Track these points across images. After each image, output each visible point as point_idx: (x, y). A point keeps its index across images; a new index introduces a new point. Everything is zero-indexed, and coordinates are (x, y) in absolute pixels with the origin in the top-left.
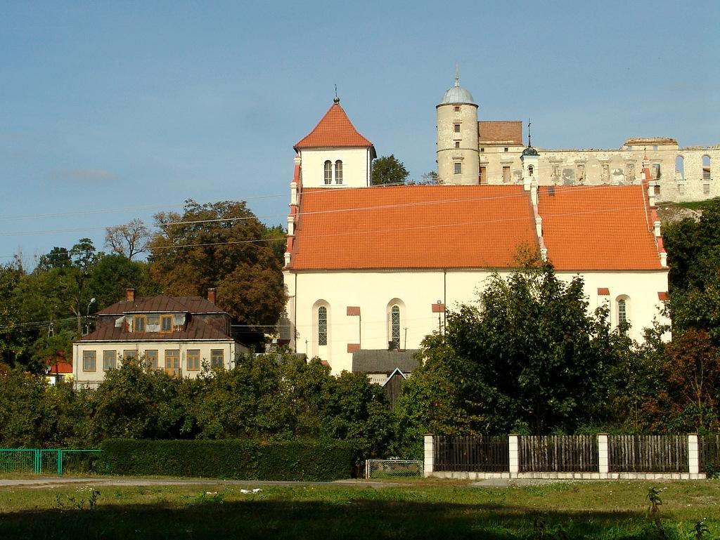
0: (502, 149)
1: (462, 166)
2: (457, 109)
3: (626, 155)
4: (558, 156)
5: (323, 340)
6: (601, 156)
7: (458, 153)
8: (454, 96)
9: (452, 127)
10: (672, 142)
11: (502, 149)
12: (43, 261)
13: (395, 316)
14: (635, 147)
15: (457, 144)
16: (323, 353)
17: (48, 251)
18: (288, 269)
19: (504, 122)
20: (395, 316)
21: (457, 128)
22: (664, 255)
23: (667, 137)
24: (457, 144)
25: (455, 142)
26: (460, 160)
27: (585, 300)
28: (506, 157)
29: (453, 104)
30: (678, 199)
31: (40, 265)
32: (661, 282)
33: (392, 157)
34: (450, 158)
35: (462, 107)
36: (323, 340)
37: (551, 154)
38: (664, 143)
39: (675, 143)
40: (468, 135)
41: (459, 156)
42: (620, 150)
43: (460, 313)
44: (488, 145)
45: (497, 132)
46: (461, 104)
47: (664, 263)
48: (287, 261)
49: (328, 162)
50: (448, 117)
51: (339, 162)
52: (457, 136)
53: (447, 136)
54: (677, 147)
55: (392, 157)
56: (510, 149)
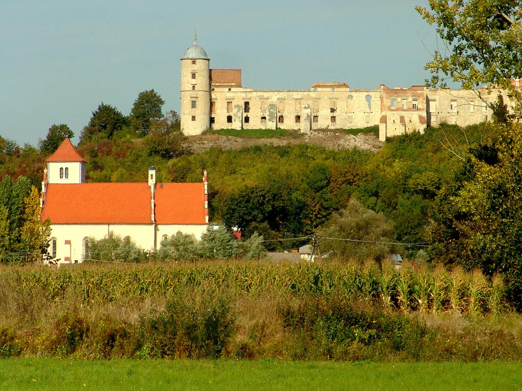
0: (227, 89)
1: (197, 103)
2: (194, 62)
3: (313, 95)
4: (266, 95)
6: (296, 95)
7: (194, 94)
8: (192, 53)
9: (190, 75)
10: (345, 85)
11: (227, 89)
14: (319, 89)
15: (194, 87)
21: (194, 76)
23: (341, 83)
24: (194, 87)
28: (230, 95)
29: (191, 59)
33: (153, 91)
34: (188, 97)
35: (197, 61)
37: (259, 94)
38: (339, 86)
39: (347, 86)
40: (201, 81)
41: (195, 96)
47: (207, 221)
51: (67, 168)
52: (194, 81)
54: (348, 89)
55: (153, 91)
56: (233, 89)
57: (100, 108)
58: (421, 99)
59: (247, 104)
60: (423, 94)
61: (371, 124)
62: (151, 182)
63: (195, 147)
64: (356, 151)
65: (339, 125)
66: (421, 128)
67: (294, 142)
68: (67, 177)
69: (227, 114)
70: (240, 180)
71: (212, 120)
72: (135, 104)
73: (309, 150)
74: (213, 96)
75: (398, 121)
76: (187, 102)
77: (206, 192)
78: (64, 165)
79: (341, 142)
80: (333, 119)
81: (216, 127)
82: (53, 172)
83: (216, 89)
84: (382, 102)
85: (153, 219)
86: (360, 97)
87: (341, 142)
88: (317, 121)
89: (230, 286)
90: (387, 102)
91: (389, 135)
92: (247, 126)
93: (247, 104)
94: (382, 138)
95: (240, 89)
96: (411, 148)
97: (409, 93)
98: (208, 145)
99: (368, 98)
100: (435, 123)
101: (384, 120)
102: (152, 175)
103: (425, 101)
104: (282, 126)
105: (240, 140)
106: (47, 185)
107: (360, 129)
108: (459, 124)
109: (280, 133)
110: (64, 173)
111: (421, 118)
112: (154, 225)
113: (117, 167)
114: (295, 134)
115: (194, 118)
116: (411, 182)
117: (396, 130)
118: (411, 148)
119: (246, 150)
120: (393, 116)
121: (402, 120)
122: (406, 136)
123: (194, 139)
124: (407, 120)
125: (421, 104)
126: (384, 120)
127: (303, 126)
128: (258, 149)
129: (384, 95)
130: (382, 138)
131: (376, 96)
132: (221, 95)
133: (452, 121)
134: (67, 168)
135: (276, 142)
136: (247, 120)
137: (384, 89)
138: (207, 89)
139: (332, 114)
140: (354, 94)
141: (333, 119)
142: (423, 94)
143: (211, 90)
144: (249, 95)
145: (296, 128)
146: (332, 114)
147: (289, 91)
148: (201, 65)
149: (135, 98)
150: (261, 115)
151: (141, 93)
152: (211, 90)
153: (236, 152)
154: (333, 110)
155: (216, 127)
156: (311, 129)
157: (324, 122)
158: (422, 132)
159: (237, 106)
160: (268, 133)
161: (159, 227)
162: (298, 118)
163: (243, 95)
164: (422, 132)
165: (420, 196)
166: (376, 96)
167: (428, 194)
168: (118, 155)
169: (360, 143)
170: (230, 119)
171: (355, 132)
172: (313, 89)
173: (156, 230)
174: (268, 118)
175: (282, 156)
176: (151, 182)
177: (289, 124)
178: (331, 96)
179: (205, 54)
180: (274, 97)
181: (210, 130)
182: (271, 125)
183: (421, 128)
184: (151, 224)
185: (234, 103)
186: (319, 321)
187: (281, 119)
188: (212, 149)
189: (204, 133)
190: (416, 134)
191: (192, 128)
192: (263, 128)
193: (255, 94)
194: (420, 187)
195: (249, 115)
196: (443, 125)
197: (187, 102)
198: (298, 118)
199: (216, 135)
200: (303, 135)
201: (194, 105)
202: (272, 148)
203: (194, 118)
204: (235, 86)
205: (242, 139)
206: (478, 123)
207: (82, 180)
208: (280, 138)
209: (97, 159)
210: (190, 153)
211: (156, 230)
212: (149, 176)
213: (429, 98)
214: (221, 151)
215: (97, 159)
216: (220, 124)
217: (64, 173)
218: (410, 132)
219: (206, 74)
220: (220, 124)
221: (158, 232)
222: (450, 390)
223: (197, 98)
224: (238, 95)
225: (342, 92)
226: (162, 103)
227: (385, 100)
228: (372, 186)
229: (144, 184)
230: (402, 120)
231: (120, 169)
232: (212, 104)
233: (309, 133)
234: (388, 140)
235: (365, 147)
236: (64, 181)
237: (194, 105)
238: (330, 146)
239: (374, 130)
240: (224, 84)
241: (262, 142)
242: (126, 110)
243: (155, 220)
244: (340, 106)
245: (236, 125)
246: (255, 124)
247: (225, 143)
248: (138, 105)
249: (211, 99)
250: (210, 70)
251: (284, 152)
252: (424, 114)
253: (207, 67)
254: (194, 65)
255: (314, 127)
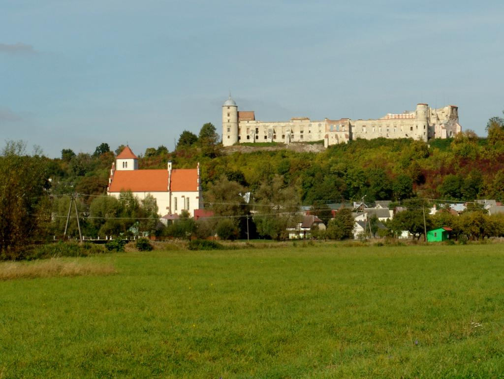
0: (246, 122)
2: (229, 108)
3: (291, 124)
4: (267, 124)
6: (283, 124)
7: (229, 124)
8: (228, 103)
9: (227, 115)
10: (307, 119)
11: (246, 122)
12: (97, 149)
14: (294, 121)
15: (229, 121)
16: (176, 212)
17: (99, 145)
19: (248, 112)
21: (229, 115)
22: (198, 188)
23: (306, 117)
24: (229, 121)
27: (128, 204)
28: (248, 125)
30: (309, 140)
31: (96, 151)
32: (197, 194)
33: (210, 123)
34: (226, 126)
37: (264, 124)
38: (305, 119)
39: (309, 119)
40: (233, 117)
42: (289, 122)
44: (242, 120)
47: (198, 190)
49: (124, 162)
50: (225, 111)
51: (126, 162)
52: (229, 118)
53: (225, 118)
54: (309, 121)
55: (210, 123)
56: (250, 122)
57: (184, 133)
58: (346, 126)
59: (257, 129)
60: (347, 123)
61: (322, 139)
62: (169, 169)
63: (228, 152)
64: (311, 153)
65: (305, 139)
66: (346, 141)
67: (280, 148)
68: (126, 167)
69: (247, 135)
70: (248, 169)
71: (239, 138)
73: (286, 152)
74: (240, 125)
75: (334, 137)
76: (225, 129)
77: (198, 174)
78: (125, 161)
79: (305, 148)
80: (302, 136)
81: (241, 141)
82: (119, 163)
83: (241, 122)
84: (326, 127)
85: (169, 189)
86: (315, 125)
87: (305, 148)
88: (293, 138)
89: (44, 226)
90: (329, 128)
91: (329, 144)
92: (257, 141)
93: (257, 129)
94: (326, 146)
95: (254, 122)
96: (340, 151)
97: (340, 122)
98: (235, 150)
99: (320, 125)
100: (354, 138)
101: (327, 136)
103: (348, 126)
104: (275, 141)
105: (252, 148)
106: (114, 172)
107: (203, 128)
108: (367, 138)
109: (273, 144)
110: (125, 165)
111: (346, 135)
112: (169, 192)
113: (185, 163)
114: (281, 145)
115: (229, 137)
116: (332, 168)
117: (333, 142)
118: (340, 151)
119: (253, 153)
120: (332, 135)
121: (336, 136)
122: (338, 145)
123: (228, 148)
124: (339, 136)
125: (347, 128)
126: (327, 136)
127: (286, 141)
128: (260, 152)
129: (327, 123)
130: (326, 146)
131: (323, 124)
132: (243, 125)
133: (363, 137)
134: (126, 162)
135: (270, 149)
136: (257, 137)
137: (327, 121)
138: (236, 121)
139: (301, 134)
140: (312, 123)
141: (302, 136)
142: (347, 123)
143: (238, 122)
144: (258, 125)
145: (282, 141)
146: (301, 134)
147: (279, 122)
148: (232, 109)
149: (201, 127)
150: (264, 135)
152: (238, 122)
153: (248, 154)
154: (302, 132)
155: (241, 141)
156: (290, 142)
157: (297, 138)
158: (346, 143)
159: (252, 130)
160: (268, 144)
161: (173, 193)
162: (283, 136)
163: (255, 125)
164: (346, 143)
165: (336, 176)
166: (323, 124)
167: (340, 175)
168: (188, 156)
169: (314, 149)
170: (248, 137)
171: (312, 143)
172: (291, 121)
173: (171, 194)
174: (268, 136)
175: (272, 156)
176: (169, 169)
177: (279, 140)
178: (301, 125)
179: (235, 104)
180: (271, 126)
181: (238, 143)
182: (269, 140)
183: (346, 141)
184: (167, 191)
185: (250, 129)
187: (275, 137)
188: (236, 153)
189: (234, 145)
190: (343, 144)
191: (228, 142)
192: (266, 142)
193: (261, 124)
194: (336, 171)
195: (258, 135)
196: (358, 139)
197: (225, 129)
198: (283, 136)
199: (240, 146)
200: (285, 145)
201: (229, 130)
202: (267, 152)
203: (229, 137)
204: (251, 120)
205: (253, 148)
206: (376, 138)
207: (135, 168)
208: (273, 147)
209: (175, 159)
210: (225, 155)
211: (171, 194)
213: (352, 125)
214: (240, 154)
215: (175, 159)
216: (244, 140)
217: (125, 165)
218: (340, 142)
219: (235, 114)
220: (244, 140)
221: (172, 196)
224: (252, 125)
225: (307, 122)
226: (215, 129)
227: (327, 126)
228: (311, 171)
229: (165, 170)
230: (336, 136)
231: (186, 164)
232: (239, 130)
233: (288, 144)
234: (329, 147)
235: (317, 151)
236: (125, 169)
237: (229, 130)
238: (298, 150)
239: (322, 142)
241: (265, 148)
242: (196, 132)
243: (170, 190)
244: (306, 130)
245: (251, 140)
246: (261, 140)
247: (244, 150)
249: (238, 127)
250: (238, 113)
251: (273, 154)
252: (348, 133)
253: (235, 110)
255: (292, 140)
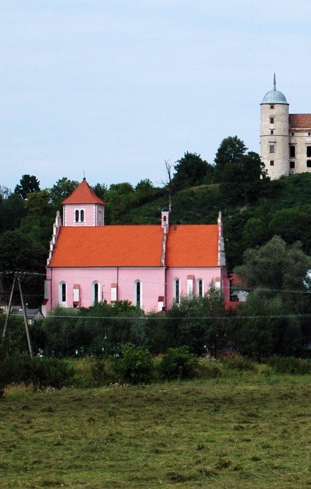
0: (307, 134)
1: (275, 147)
2: (272, 108)
5: (64, 299)
7: (272, 138)
11: (307, 134)
13: (275, 76)
15: (272, 132)
18: (48, 267)
20: (275, 76)
21: (272, 121)
24: (272, 132)
25: (270, 131)
26: (274, 144)
29: (269, 104)
34: (267, 141)
35: (276, 106)
36: (64, 299)
41: (274, 141)
43: (232, 347)
45: (303, 121)
46: (275, 104)
48: (48, 263)
52: (272, 126)
72: (219, 150)
91: (74, 301)
102: (165, 217)
110: (79, 216)
151: (224, 139)
179: (284, 98)
186: (27, 476)
212: (167, 219)
217: (79, 216)
222: (299, 488)
223: (275, 142)
229: (157, 227)
240: (304, 129)
248: (222, 152)
254: (272, 110)
